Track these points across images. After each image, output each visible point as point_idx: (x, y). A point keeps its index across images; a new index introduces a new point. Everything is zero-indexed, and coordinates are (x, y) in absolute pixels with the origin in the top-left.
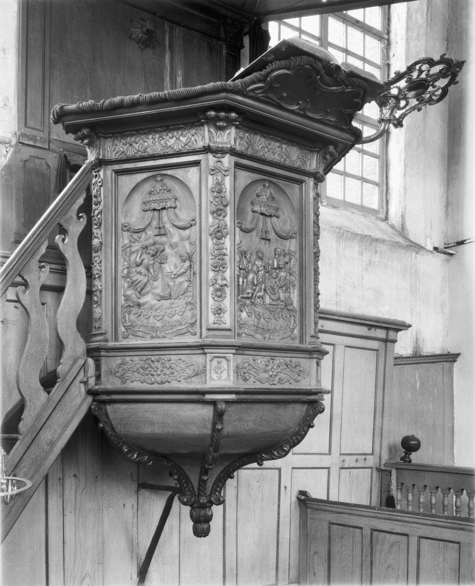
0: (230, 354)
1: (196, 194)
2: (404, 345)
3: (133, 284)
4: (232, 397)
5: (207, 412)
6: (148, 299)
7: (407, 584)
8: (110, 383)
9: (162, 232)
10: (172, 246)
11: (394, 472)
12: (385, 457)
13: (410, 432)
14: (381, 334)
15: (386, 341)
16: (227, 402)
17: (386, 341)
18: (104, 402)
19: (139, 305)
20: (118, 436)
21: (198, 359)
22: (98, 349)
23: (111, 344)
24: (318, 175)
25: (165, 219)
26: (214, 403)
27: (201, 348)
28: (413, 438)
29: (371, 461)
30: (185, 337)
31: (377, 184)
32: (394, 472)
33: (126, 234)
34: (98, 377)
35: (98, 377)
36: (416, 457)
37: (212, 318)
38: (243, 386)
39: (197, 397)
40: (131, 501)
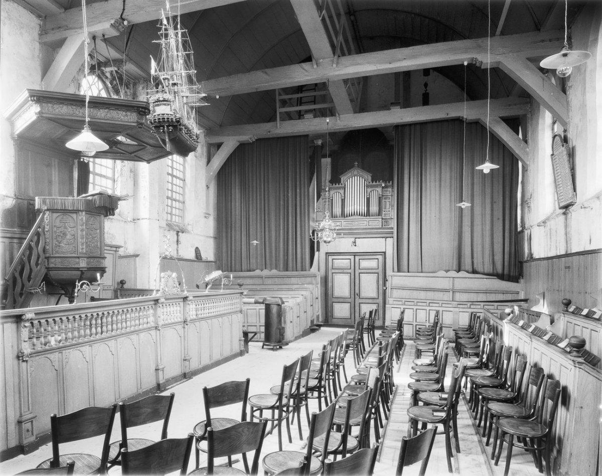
0: (85, 259)
1: (76, 220)
2: (121, 252)
3: (57, 241)
4: (86, 269)
5: (79, 273)
6: (62, 245)
7: (347, 3)
8: (52, 265)
9: (65, 228)
10: (69, 232)
11: (119, 291)
12: (116, 286)
13: (569, 187)
14: (114, 249)
15: (116, 251)
16: (85, 270)
17: (116, 251)
18: (49, 270)
19: (59, 246)
20: (52, 279)
21: (77, 260)
22: (49, 257)
23: (52, 256)
24: (104, 212)
25: (66, 225)
26: (81, 271)
27: (78, 258)
28: (123, 280)
29: (112, 288)
30: (521, 332)
31: (96, 185)
32: (119, 291)
33: (55, 228)
34: (48, 264)
35: (48, 264)
36: (125, 286)
37: (81, 250)
38: (89, 267)
39: (78, 269)
40: (46, 298)
